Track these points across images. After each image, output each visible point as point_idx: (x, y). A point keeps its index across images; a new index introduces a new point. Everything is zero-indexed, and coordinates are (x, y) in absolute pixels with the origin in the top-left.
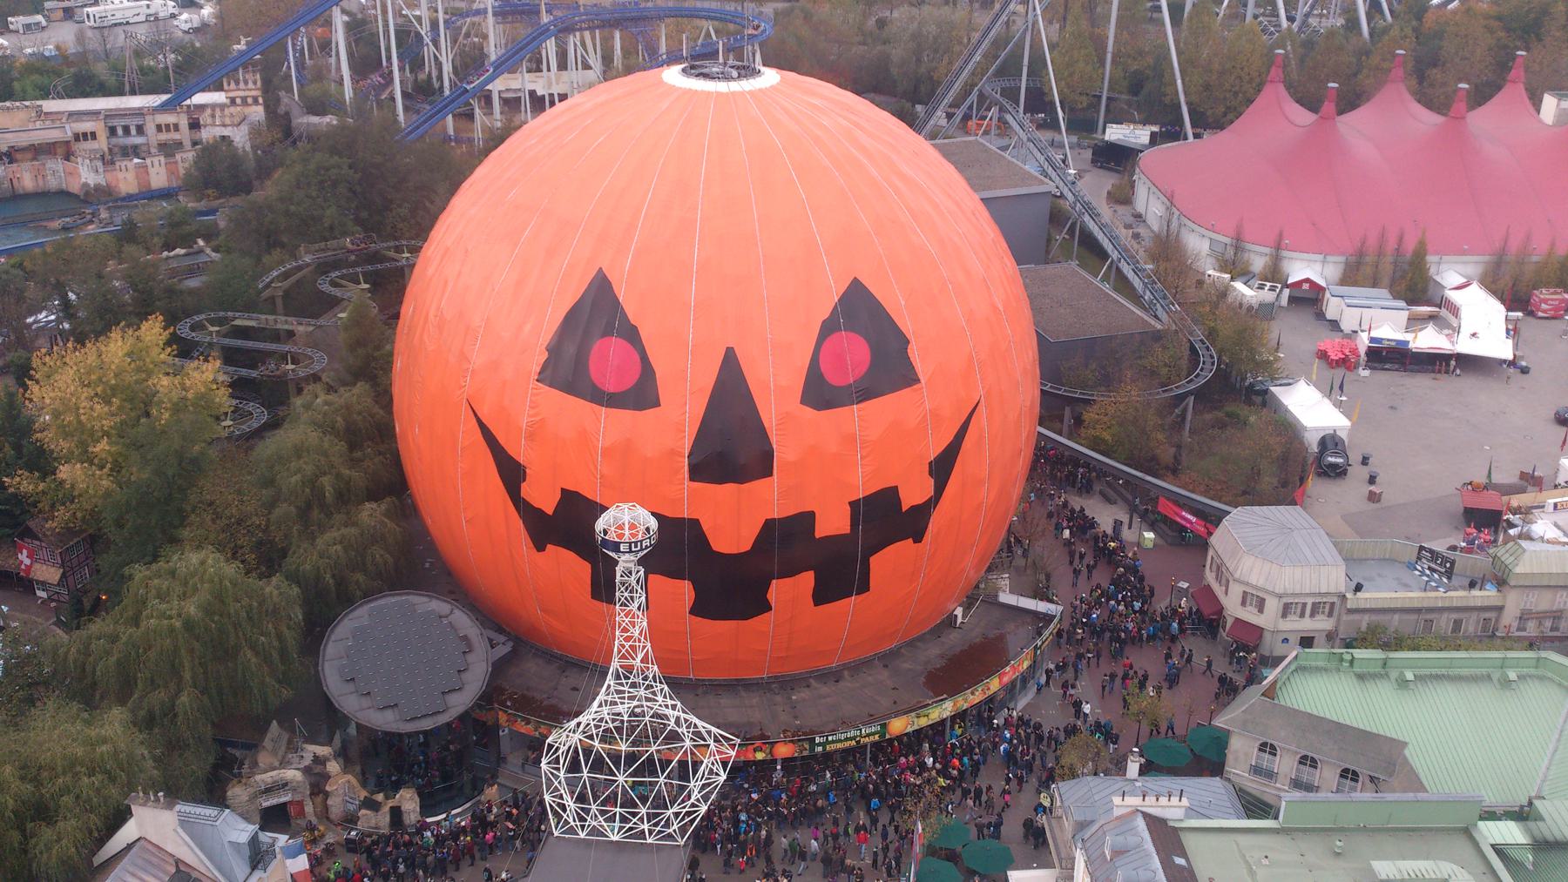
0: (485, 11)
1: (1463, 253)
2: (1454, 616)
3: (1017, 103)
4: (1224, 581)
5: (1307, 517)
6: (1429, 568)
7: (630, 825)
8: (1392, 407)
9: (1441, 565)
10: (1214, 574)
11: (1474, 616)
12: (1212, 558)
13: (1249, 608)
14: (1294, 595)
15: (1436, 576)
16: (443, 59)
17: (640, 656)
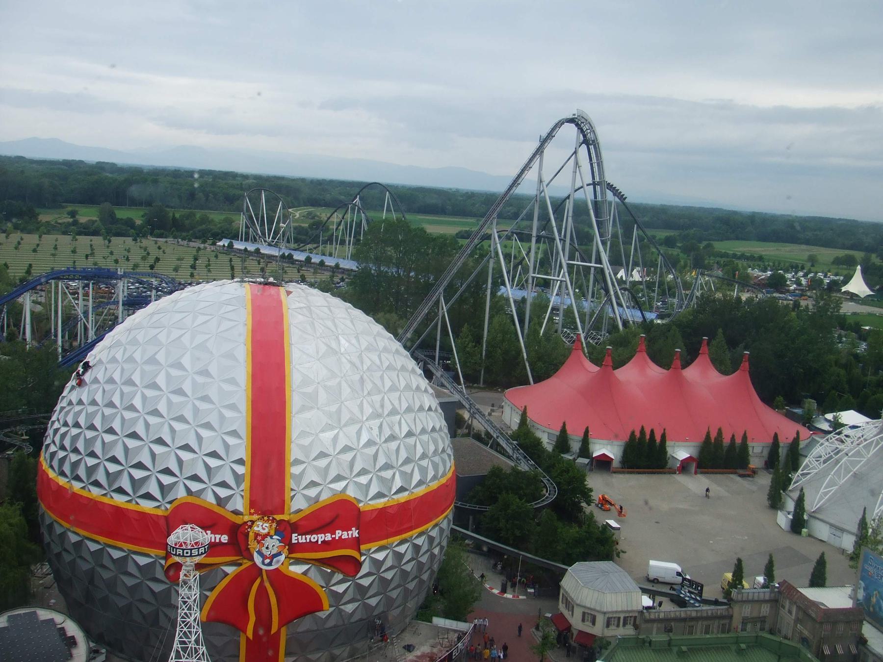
0: (118, 302)
1: (687, 441)
2: (705, 623)
3: (434, 360)
4: (570, 609)
5: (617, 567)
6: (689, 592)
7: (186, 640)
8: (657, 522)
9: (695, 589)
10: (564, 605)
11: (716, 623)
12: (563, 594)
13: (587, 623)
14: (613, 612)
15: (693, 596)
16: (89, 326)
17: (193, 638)
